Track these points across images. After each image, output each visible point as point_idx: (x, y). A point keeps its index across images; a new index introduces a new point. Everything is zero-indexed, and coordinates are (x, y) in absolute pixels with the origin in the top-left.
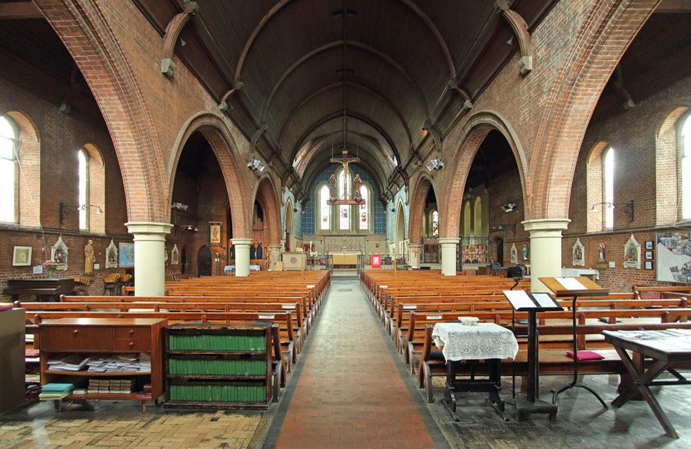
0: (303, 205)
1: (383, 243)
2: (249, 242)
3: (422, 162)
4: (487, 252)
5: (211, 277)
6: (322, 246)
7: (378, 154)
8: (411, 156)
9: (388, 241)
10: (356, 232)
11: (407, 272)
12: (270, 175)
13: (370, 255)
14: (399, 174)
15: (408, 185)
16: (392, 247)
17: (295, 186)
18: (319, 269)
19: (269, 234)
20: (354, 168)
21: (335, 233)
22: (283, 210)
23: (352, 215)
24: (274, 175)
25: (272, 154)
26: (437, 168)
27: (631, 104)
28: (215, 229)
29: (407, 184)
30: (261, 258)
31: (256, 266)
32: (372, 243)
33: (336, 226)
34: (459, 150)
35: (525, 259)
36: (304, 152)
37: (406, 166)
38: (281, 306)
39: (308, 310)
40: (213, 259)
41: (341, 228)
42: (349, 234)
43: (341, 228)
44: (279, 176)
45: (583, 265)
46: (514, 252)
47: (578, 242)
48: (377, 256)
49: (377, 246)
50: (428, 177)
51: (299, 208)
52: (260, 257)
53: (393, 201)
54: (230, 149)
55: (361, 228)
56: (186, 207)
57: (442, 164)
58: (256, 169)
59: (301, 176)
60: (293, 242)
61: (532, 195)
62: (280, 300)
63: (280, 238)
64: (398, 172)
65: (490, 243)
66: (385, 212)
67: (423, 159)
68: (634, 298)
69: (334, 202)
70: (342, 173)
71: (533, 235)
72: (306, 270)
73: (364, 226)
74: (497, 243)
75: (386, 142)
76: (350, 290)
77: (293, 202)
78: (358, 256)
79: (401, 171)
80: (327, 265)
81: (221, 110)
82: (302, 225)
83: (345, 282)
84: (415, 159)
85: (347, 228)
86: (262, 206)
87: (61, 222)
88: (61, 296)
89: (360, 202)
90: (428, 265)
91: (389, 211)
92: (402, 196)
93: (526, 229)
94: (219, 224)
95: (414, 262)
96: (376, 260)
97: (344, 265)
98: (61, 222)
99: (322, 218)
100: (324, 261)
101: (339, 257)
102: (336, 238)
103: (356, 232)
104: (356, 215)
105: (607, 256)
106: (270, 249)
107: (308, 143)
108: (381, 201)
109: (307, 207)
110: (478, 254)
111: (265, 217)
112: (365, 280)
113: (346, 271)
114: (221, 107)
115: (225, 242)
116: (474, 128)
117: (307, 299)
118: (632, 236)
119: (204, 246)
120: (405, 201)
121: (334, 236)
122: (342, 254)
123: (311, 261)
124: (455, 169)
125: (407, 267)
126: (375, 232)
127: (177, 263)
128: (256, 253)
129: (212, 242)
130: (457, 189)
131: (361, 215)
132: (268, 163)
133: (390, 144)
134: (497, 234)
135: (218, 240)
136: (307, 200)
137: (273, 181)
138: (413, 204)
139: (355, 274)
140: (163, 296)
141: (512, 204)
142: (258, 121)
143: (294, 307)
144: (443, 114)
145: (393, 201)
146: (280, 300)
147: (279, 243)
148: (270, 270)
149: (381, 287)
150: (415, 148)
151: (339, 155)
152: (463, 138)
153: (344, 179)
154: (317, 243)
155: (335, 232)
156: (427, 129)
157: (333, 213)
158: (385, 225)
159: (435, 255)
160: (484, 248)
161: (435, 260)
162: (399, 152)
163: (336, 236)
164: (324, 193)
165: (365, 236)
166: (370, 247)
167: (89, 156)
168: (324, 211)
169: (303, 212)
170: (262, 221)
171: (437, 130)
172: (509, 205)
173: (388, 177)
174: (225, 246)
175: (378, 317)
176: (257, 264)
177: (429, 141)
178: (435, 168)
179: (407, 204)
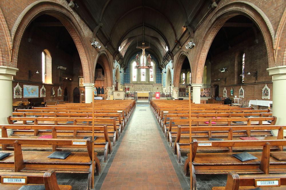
0: (125, 70)
1: (160, 87)
3: (182, 47)
4: (210, 91)
5: (78, 104)
6: (133, 88)
7: (159, 46)
8: (176, 43)
9: (163, 86)
10: (148, 83)
11: (171, 101)
12: (106, 52)
14: (169, 55)
15: (173, 59)
16: (164, 89)
17: (120, 60)
18: (131, 99)
19: (107, 82)
20: (147, 52)
22: (114, 71)
23: (147, 74)
24: (109, 53)
25: (107, 41)
26: (191, 47)
27: (230, 47)
29: (173, 59)
30: (103, 94)
31: (101, 97)
34: (206, 35)
35: (232, 95)
36: (125, 44)
37: (173, 50)
38: (71, 142)
39: (127, 113)
40: (80, 94)
41: (142, 80)
42: (145, 83)
43: (142, 80)
44: (111, 54)
45: (269, 99)
46: (225, 91)
47: (242, 88)
48: (158, 93)
49: (158, 89)
50: (185, 53)
51: (122, 70)
52: (103, 93)
53: (165, 68)
54: (79, 32)
55: (150, 81)
56: (65, 68)
57: (194, 45)
58: (97, 47)
59: (123, 56)
60: (120, 86)
61: (278, 48)
62: (81, 129)
63: (112, 84)
64: (169, 53)
65: (212, 87)
66: (161, 74)
67: (182, 45)
68: (268, 112)
69: (138, 68)
70: (142, 56)
71: (193, 88)
72: (124, 99)
74: (215, 87)
75: (163, 39)
76: (145, 110)
77: (119, 68)
78: (149, 93)
79: (170, 54)
80: (134, 97)
81: (71, 7)
82: (124, 79)
83: (143, 105)
84: (178, 45)
85: (144, 81)
86: (104, 69)
87: (30, 78)
88: (32, 107)
89: (150, 67)
90: (182, 98)
92: (170, 65)
93: (270, 74)
95: (175, 96)
96: (158, 95)
97: (143, 97)
98: (30, 78)
100: (134, 95)
101: (140, 93)
102: (139, 85)
103: (148, 83)
104: (148, 75)
105: (234, 94)
106: (107, 89)
107: (127, 39)
108: (159, 69)
110: (204, 93)
111: (105, 74)
112: (152, 104)
113: (144, 100)
114: (70, 4)
116: (217, 19)
117: (127, 109)
118: (266, 85)
119: (76, 87)
120: (171, 67)
121: (138, 84)
122: (142, 92)
123: (127, 95)
124: (203, 46)
125: (172, 98)
126: (157, 82)
127: (61, 96)
128: (100, 91)
129: (80, 86)
130: (203, 58)
131: (150, 75)
132: (105, 46)
133: (165, 41)
134: (216, 83)
136: (126, 67)
137: (108, 56)
138: (176, 68)
139: (147, 101)
140: (90, 103)
141: (225, 68)
142: (97, 20)
143: (85, 144)
144: (195, 18)
145: (165, 68)
146: (84, 129)
147: (112, 86)
148: (107, 99)
149: (164, 112)
150: (178, 39)
151: (141, 45)
152: (209, 26)
153: (143, 58)
154: (131, 87)
155: (139, 83)
156: (186, 26)
157: (138, 74)
158: (161, 79)
159: (184, 93)
160: (208, 89)
161: (184, 95)
163: (139, 84)
164: (134, 64)
165: (152, 84)
166: (155, 90)
167: (45, 54)
168: (134, 72)
169: (125, 73)
170: (104, 76)
171: (192, 27)
172: (224, 69)
173: (163, 56)
175: (162, 132)
176: (101, 97)
177: (187, 33)
178: (189, 48)
179: (172, 69)
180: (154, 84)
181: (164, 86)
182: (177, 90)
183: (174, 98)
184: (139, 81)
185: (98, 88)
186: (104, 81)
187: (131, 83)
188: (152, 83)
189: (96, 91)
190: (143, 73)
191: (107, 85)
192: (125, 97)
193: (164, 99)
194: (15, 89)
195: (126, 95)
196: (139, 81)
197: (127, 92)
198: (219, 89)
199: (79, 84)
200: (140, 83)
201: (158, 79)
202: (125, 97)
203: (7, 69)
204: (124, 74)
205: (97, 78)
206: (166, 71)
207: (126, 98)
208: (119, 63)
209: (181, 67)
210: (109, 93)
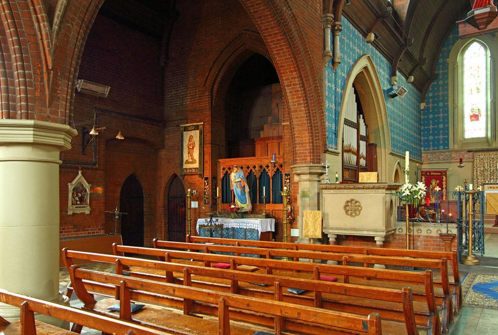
2: (60, 140)
19: (293, 144)
28: (191, 138)
82: (419, 132)
94: (197, 128)
99: (467, 113)
106: (296, 178)
109: (431, 95)
115: (208, 167)
129: (185, 166)
135: (194, 162)
154: (452, 168)
169: (423, 106)
174: (208, 174)
185: (257, 173)
186: (280, 138)
187: (456, 147)
189: (247, 189)
191: (294, 153)
192: (401, 219)
194: (71, 187)
195: (401, 209)
197: (407, 192)
199: (182, 161)
202: (401, 219)
203: (34, 130)
204: (419, 111)
205: (265, 126)
207: (402, 228)
208: (374, 44)
210: (304, 195)
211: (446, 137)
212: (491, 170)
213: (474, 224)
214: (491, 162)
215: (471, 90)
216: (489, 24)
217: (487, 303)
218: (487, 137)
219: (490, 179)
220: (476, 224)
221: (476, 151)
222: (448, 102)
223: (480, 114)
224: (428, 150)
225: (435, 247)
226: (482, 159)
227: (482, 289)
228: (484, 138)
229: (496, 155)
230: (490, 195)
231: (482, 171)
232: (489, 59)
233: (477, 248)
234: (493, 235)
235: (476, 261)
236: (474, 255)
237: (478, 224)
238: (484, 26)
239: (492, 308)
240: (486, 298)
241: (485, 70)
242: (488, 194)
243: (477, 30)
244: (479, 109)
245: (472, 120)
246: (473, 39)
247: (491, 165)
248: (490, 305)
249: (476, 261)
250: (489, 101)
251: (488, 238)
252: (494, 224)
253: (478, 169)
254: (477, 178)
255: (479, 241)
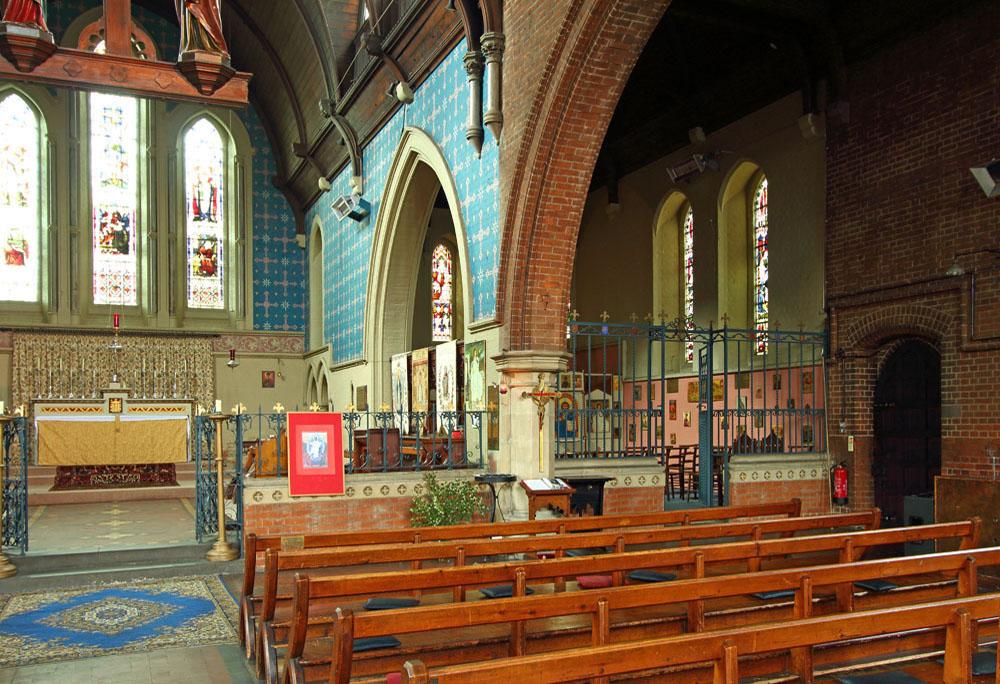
1: (292, 371)
13: (276, 417)
21: (59, 320)
32: (251, 369)
33: (73, 287)
53: (358, 172)
55: (193, 303)
66: (301, 239)
73: (206, 293)
91: (328, 216)
96: (314, 445)
97: (115, 469)
102: (73, 342)
104: (172, 242)
126: (259, 321)
131: (193, 245)
139: (175, 530)
158: (301, 295)
162: (305, 114)
165: (216, 336)
180: (236, 334)
181: (335, 358)
182: (544, 388)
183: (509, 480)
184: (64, 300)
188: (213, 328)
190: (119, 227)
193: (393, 493)
196: (64, 300)
198: (947, 370)
200: (76, 323)
201: (276, 294)
206: (373, 196)
209: (606, 103)
211: (258, 304)
212: (48, 372)
213: (7, 488)
214: (49, 357)
215: (8, 197)
216: (39, 65)
217: (28, 653)
218: (140, 306)
219: (47, 392)
220: (12, 487)
221: (18, 330)
222: (254, 240)
223: (26, 251)
224: (279, 329)
225: (987, 431)
226: (30, 348)
227: (19, 626)
228: (34, 303)
229: (59, 341)
230: (45, 423)
231: (30, 374)
232: (45, 140)
233: (12, 540)
234: (51, 508)
235: (11, 567)
236: (6, 555)
237: (16, 487)
238: (28, 66)
239: (36, 661)
240: (26, 643)
241: (36, 161)
242: (43, 422)
243: (13, 67)
244: (23, 241)
245: (9, 263)
246: (10, 86)
247: (49, 363)
248: (32, 657)
249: (11, 567)
250: (45, 226)
251: (40, 515)
252: (53, 485)
253: (23, 368)
254: (19, 388)
255: (17, 523)
